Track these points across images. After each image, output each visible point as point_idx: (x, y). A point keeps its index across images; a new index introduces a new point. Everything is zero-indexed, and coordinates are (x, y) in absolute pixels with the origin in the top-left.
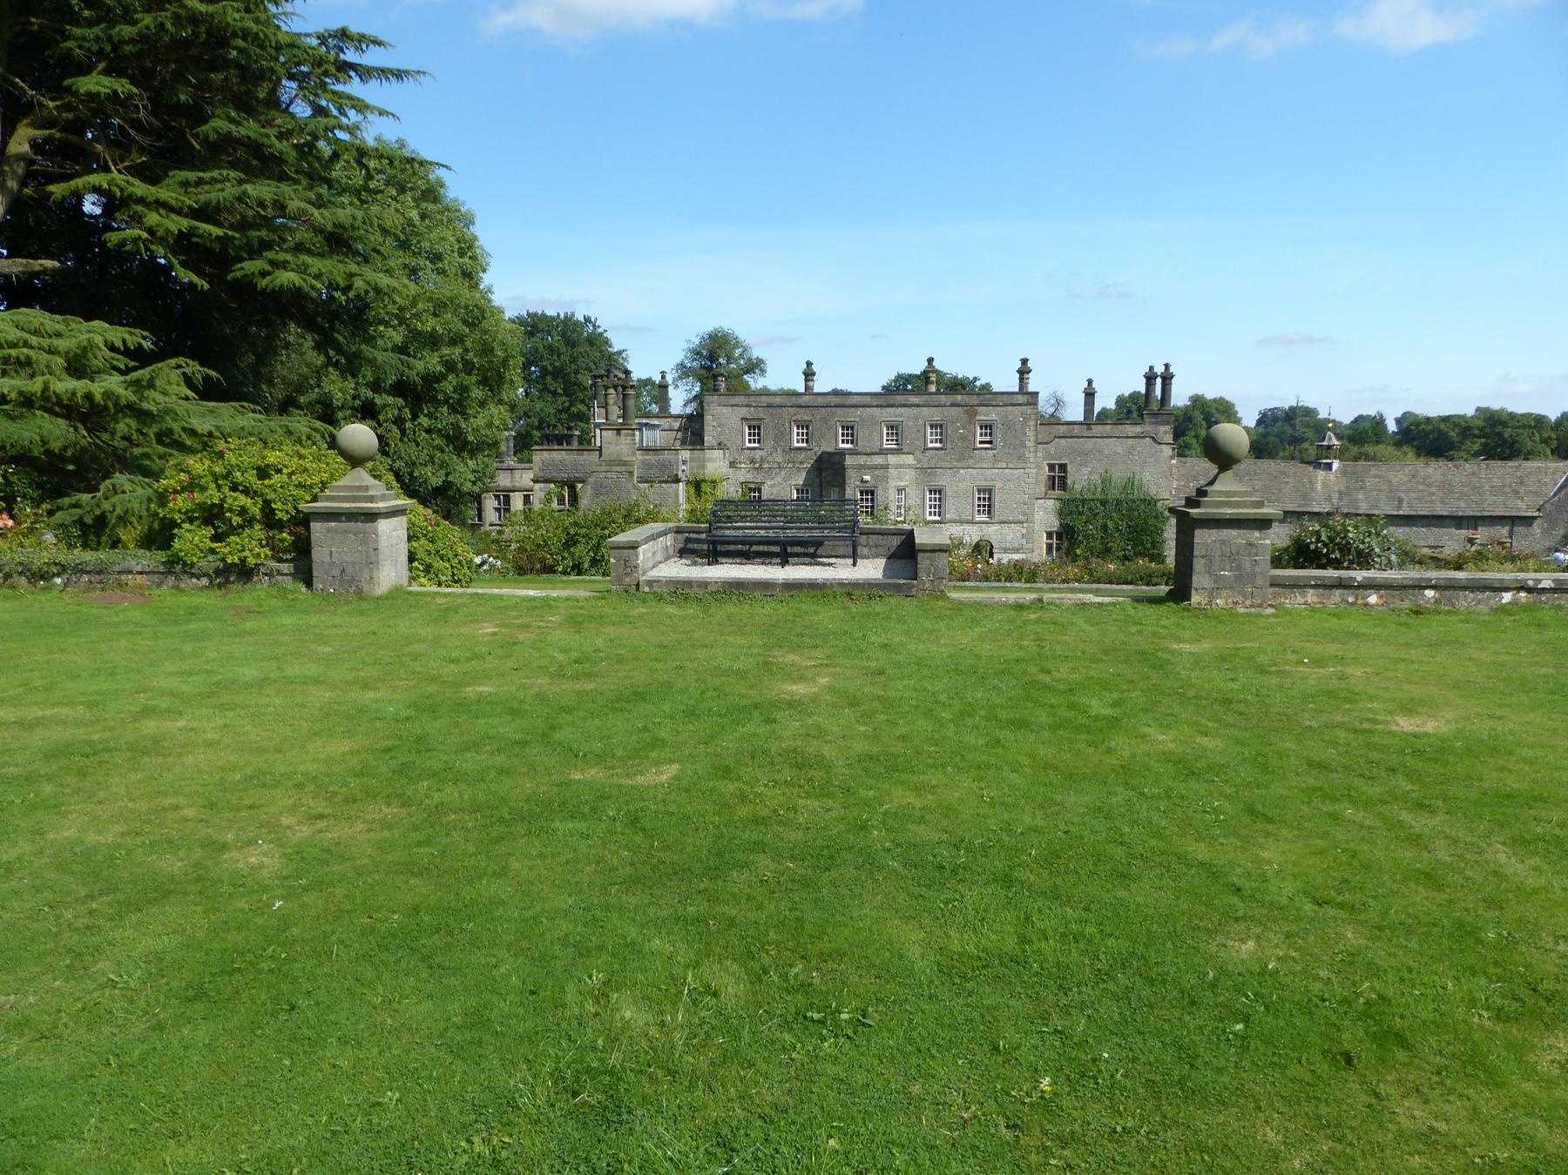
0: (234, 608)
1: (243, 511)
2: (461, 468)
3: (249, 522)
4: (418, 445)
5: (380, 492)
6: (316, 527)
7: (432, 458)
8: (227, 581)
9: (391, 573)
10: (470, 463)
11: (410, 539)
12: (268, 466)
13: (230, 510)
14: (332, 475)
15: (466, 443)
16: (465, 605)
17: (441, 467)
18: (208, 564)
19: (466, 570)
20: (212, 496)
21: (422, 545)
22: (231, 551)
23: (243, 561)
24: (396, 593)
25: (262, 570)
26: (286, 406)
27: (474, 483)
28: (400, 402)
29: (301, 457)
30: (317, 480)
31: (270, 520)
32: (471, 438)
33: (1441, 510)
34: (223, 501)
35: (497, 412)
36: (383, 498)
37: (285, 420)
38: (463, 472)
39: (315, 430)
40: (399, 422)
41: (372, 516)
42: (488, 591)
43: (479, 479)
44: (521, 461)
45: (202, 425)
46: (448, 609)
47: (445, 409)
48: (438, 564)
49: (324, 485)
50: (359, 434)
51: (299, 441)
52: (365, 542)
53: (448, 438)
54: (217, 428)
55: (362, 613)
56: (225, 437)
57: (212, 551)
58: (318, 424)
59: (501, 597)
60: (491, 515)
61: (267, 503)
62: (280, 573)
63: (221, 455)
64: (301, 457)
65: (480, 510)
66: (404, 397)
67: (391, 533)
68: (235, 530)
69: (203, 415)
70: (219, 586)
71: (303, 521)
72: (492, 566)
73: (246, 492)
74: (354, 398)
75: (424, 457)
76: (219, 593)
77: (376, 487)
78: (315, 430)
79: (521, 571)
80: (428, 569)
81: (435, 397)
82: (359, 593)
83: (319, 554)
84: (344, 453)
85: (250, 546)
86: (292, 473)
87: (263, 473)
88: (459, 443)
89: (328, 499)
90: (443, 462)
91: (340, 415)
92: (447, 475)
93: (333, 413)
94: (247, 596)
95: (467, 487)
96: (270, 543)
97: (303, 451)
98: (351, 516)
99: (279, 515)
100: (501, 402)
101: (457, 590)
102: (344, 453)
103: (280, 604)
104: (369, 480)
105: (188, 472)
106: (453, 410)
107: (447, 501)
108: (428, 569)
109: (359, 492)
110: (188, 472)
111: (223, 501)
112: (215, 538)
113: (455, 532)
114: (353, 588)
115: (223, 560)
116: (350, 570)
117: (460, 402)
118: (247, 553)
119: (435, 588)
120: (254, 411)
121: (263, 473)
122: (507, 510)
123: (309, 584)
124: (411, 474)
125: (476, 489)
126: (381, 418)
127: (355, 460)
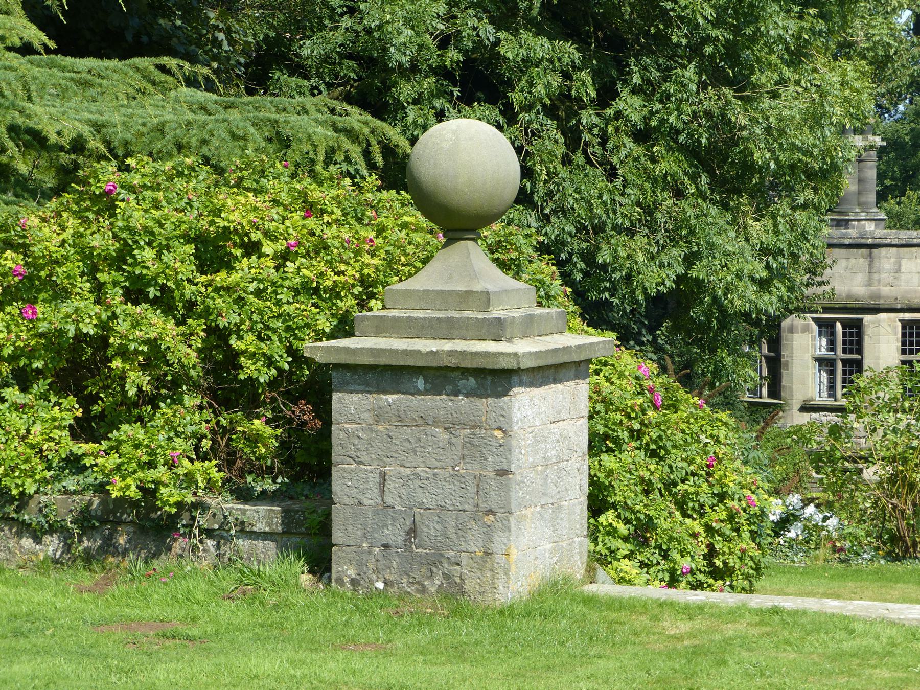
0: (127, 623)
1: (155, 356)
2: (729, 241)
3: (170, 386)
4: (612, 173)
5: (529, 318)
6: (347, 405)
7: (649, 211)
8: (108, 547)
9: (541, 539)
10: (758, 229)
11: (599, 443)
12: (225, 233)
13: (123, 353)
14: (390, 262)
15: (748, 167)
16: (745, 643)
17: (674, 239)
18: (61, 499)
19: (745, 543)
20: (78, 314)
21: (626, 464)
22: (122, 463)
23: (149, 493)
24: (551, 599)
25: (202, 520)
26: (262, 69)
27: (764, 285)
28: (569, 51)
29: (311, 209)
30: (352, 272)
31: (227, 389)
32: (760, 156)
33: (895, 249)
34: (105, 327)
35: (841, 82)
36: (528, 327)
37: (265, 106)
38: (734, 254)
39: (350, 134)
40: (562, 107)
41: (496, 379)
42: (811, 604)
43: (781, 275)
44: (896, 221)
45: (60, 119)
46: (696, 652)
47: (690, 72)
48: (668, 520)
49: (368, 289)
50: (469, 149)
51: (306, 167)
52: (474, 450)
53: (692, 152)
54: (97, 127)
55: (459, 653)
56: (119, 154)
57: (74, 464)
58: (356, 118)
59: (846, 625)
60: (805, 379)
61: (218, 336)
62: (245, 531)
63: (106, 204)
64: (311, 209)
65: (775, 364)
66: (582, 42)
67: (547, 426)
68: (137, 408)
69: (63, 94)
70: (88, 558)
71: (312, 387)
72: (812, 530)
73: (165, 302)
74: (444, 42)
75: (628, 208)
76: (86, 578)
77: (512, 297)
78: (350, 134)
79: (897, 547)
80: (642, 533)
81: (662, 39)
82: (454, 591)
83: (351, 483)
84: (432, 205)
85: (166, 451)
86: (283, 257)
87: (212, 253)
88: (726, 170)
89: (383, 327)
90: (679, 222)
91: (405, 90)
92: (690, 259)
93: (387, 87)
94: (158, 591)
95: (747, 296)
96: (224, 450)
97: (316, 194)
98: (442, 377)
99: (250, 369)
100: (846, 49)
101: (720, 597)
102: (432, 205)
103: (243, 616)
104: (494, 279)
105: (23, 249)
106: (714, 77)
107: (685, 330)
108: (642, 533)
109: (466, 311)
110: (23, 249)
111: (105, 327)
112: (83, 429)
113: (725, 432)
114: (437, 580)
115: (101, 489)
116: (430, 529)
117: (732, 52)
118: (161, 472)
119: (657, 591)
120: (191, 82)
121: (212, 253)
122: (855, 366)
123: (320, 564)
124: (589, 257)
125: (769, 303)
126: (516, 97)
127: (456, 222)
